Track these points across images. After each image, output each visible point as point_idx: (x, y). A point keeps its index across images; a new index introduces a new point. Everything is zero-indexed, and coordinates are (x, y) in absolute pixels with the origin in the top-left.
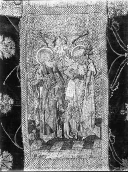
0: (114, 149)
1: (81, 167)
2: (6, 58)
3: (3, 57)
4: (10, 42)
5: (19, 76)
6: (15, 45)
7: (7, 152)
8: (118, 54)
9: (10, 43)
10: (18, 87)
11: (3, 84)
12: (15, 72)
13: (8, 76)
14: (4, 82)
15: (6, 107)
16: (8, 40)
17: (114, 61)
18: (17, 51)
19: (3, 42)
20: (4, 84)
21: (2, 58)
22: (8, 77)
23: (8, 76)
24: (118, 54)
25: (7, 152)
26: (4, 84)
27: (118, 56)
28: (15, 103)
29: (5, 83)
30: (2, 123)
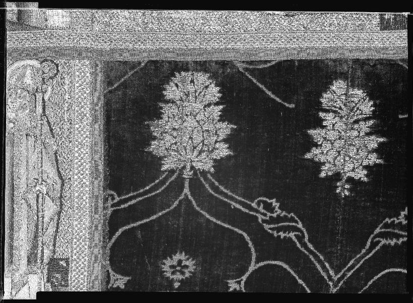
0: (326, 277)
1: (161, 290)
2: (220, 95)
3: (217, 104)
4: (177, 86)
5: (266, 62)
6: (183, 73)
7: (168, 87)
8: (261, 264)
9: (179, 85)
10: (297, 64)
11: (293, 109)
12: (252, 72)
13: (269, 93)
14: (287, 105)
15: (356, 100)
16: (171, 92)
17: (292, 273)
18: (202, 66)
19: (178, 102)
20: (292, 106)
21: (221, 107)
22: (273, 93)
23: (269, 93)
24: (261, 264)
25: (168, 87)
26: (292, 106)
27: (257, 262)
28: (343, 76)
29: (290, 103)
30: (400, 117)
